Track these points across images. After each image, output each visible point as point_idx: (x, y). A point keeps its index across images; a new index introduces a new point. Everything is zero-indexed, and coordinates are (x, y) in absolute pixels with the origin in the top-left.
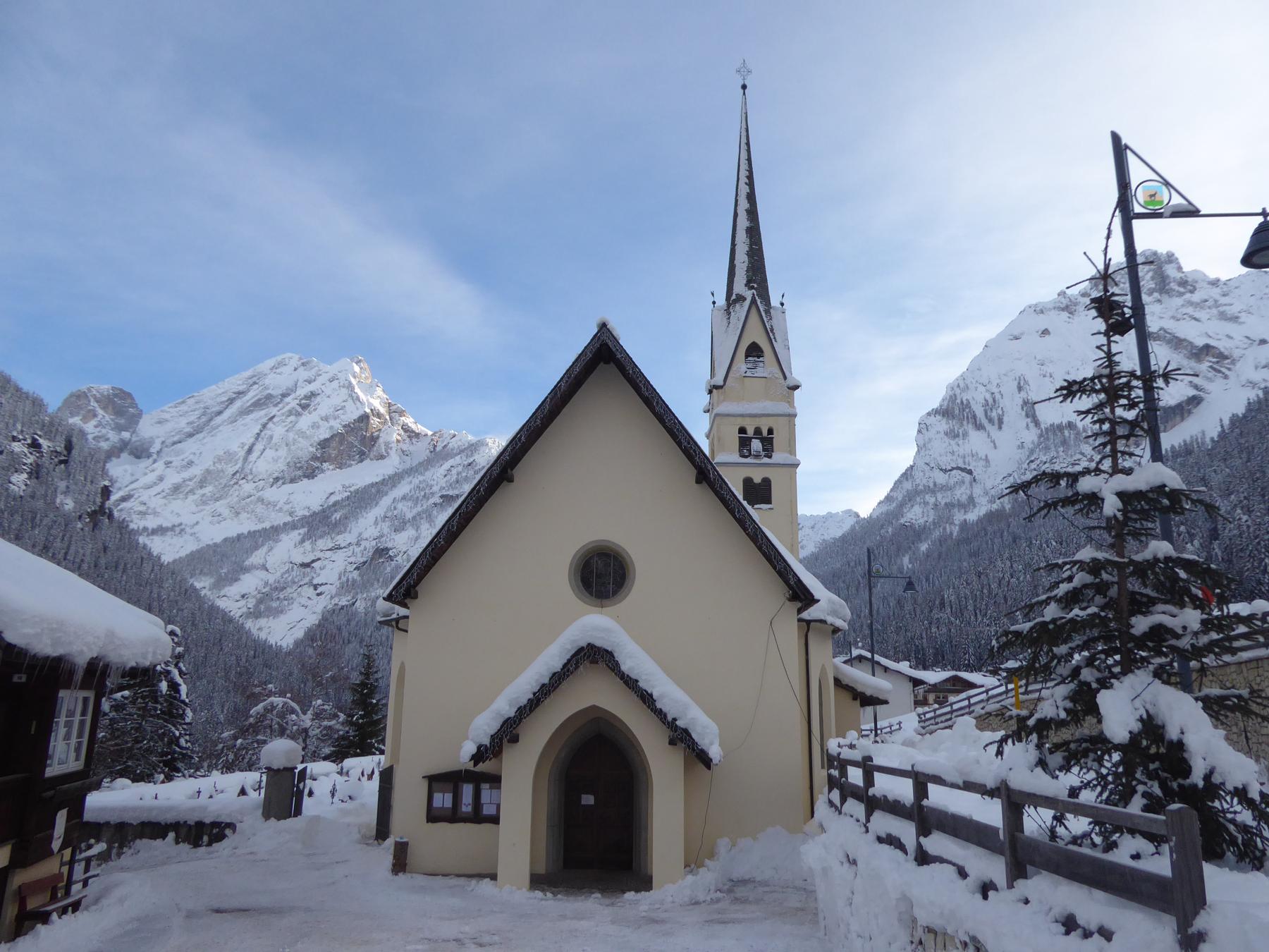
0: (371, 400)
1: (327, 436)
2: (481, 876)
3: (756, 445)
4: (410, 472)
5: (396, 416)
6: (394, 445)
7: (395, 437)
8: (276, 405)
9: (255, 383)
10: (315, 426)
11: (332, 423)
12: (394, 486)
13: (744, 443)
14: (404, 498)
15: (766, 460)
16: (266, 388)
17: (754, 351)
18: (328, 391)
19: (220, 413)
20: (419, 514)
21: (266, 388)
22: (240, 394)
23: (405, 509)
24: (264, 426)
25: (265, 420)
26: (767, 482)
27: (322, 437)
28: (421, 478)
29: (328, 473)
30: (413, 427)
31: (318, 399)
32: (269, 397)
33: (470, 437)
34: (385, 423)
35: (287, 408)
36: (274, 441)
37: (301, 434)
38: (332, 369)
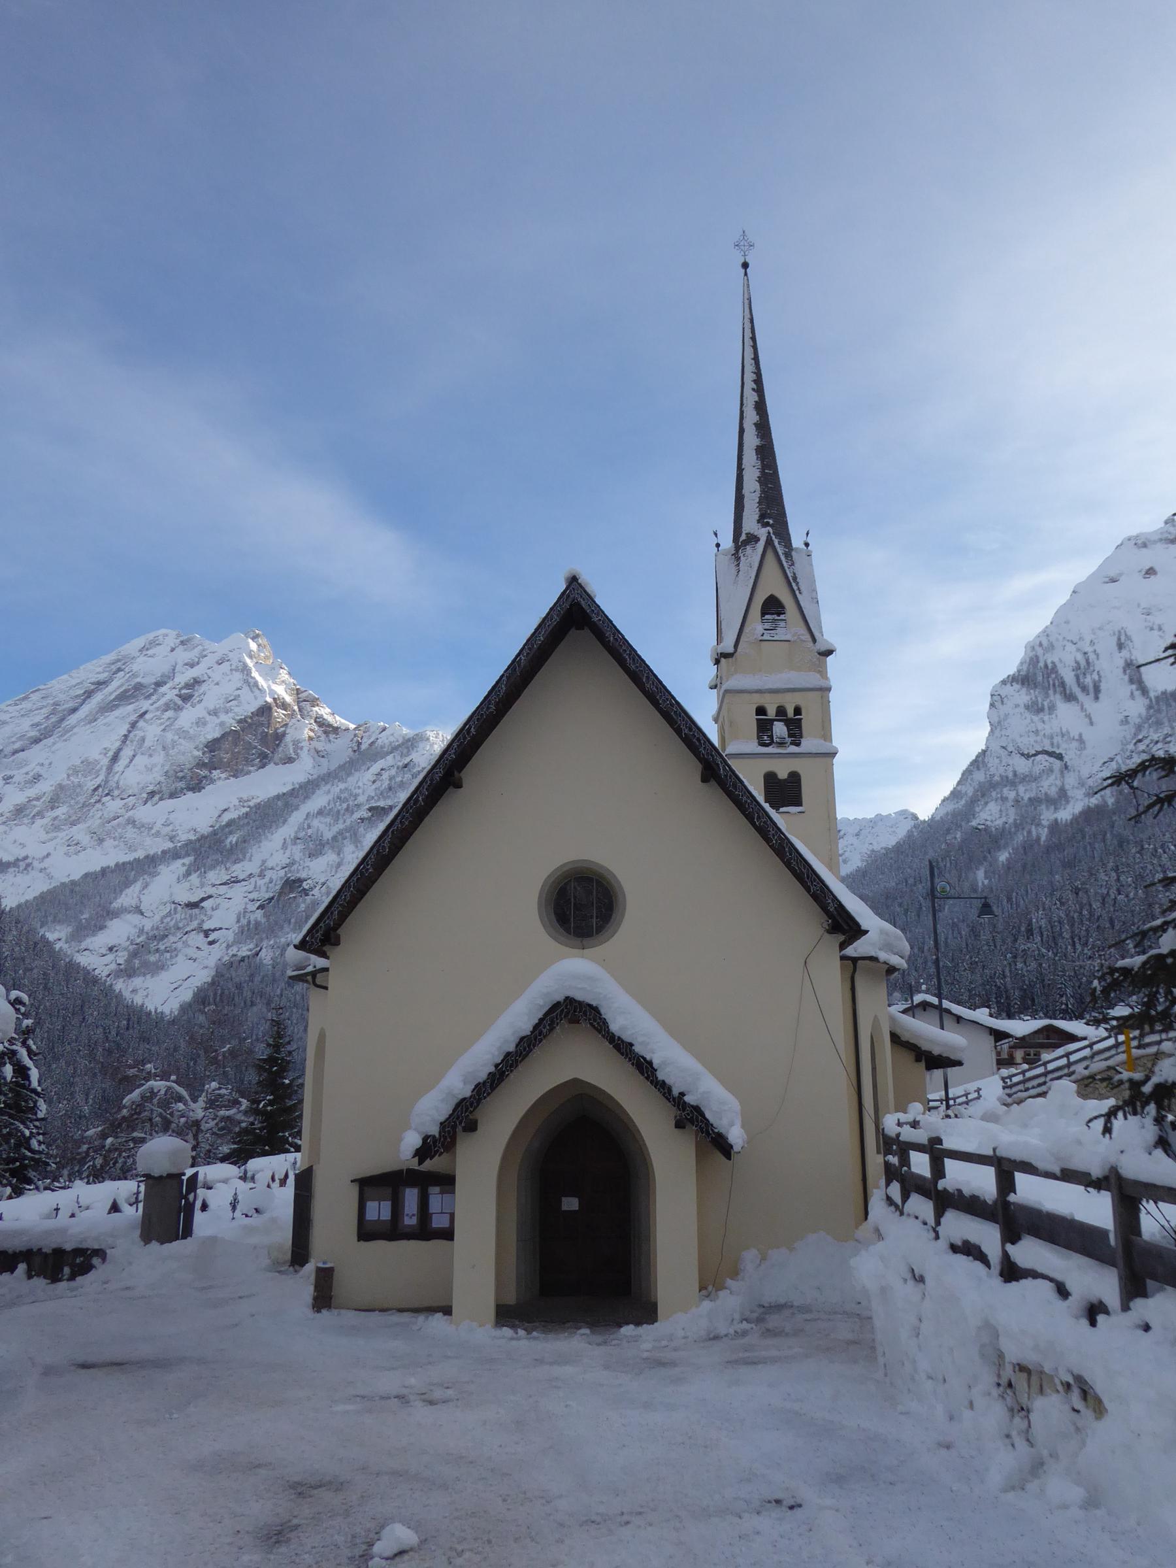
1: (217, 735)
2: (431, 1310)
3: (780, 729)
4: (328, 777)
6: (305, 744)
7: (306, 733)
8: (148, 697)
9: (119, 670)
10: (200, 723)
12: (307, 797)
13: (764, 727)
14: (320, 813)
15: (793, 749)
17: (773, 607)
19: (74, 710)
20: (340, 833)
21: (135, 676)
22: (101, 684)
23: (322, 827)
24: (133, 725)
25: (133, 717)
26: (795, 777)
27: (210, 737)
28: (342, 786)
30: (330, 719)
31: (204, 688)
32: (139, 687)
33: (405, 731)
36: (147, 744)
37: (183, 734)
38: (219, 648)
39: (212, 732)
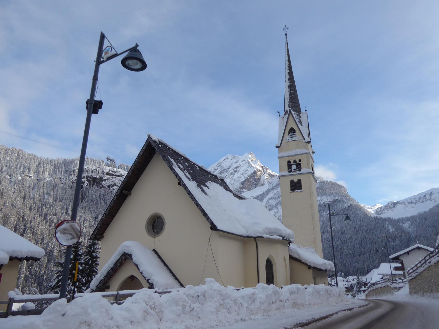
0: (256, 166)
1: (244, 180)
3: (294, 167)
4: (273, 189)
5: (265, 170)
6: (266, 180)
7: (266, 177)
8: (226, 172)
10: (239, 177)
11: (245, 175)
12: (268, 195)
13: (290, 167)
14: (271, 198)
15: (298, 172)
16: (223, 167)
17: (292, 131)
18: (242, 165)
20: (277, 203)
21: (223, 167)
23: (272, 202)
26: (299, 181)
27: (242, 181)
28: (276, 191)
29: (245, 192)
30: (272, 173)
31: (239, 168)
32: (224, 170)
34: (262, 173)
35: (230, 172)
37: (235, 180)
38: (242, 158)
39: (242, 180)
